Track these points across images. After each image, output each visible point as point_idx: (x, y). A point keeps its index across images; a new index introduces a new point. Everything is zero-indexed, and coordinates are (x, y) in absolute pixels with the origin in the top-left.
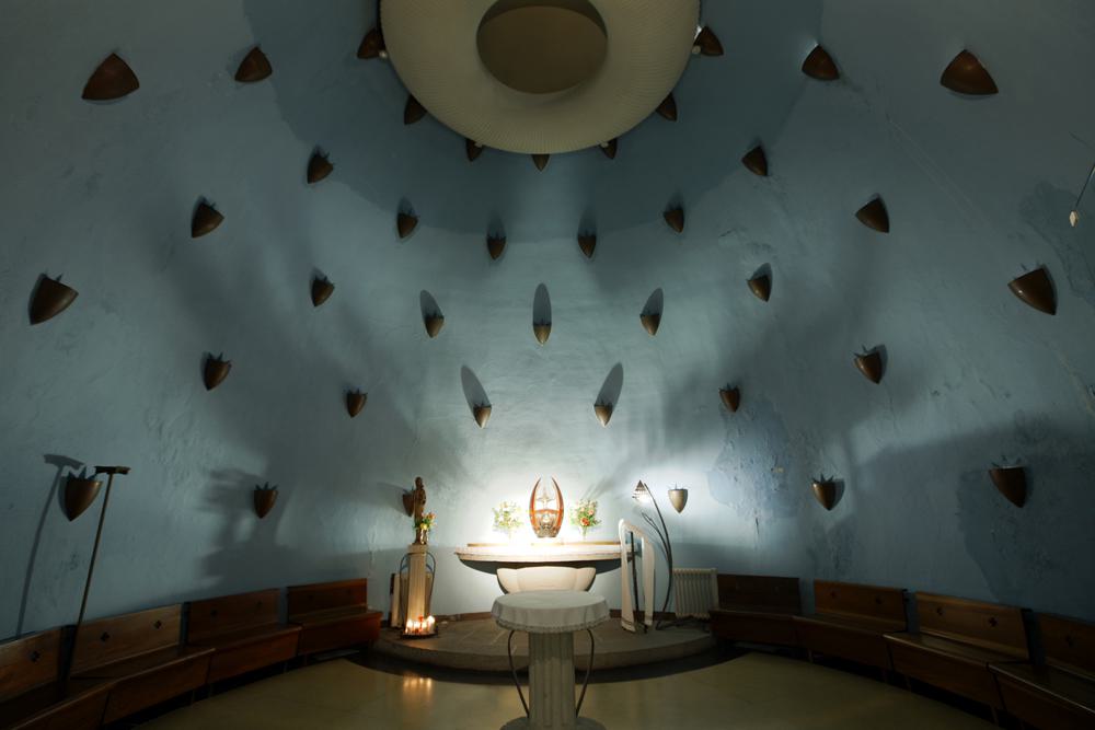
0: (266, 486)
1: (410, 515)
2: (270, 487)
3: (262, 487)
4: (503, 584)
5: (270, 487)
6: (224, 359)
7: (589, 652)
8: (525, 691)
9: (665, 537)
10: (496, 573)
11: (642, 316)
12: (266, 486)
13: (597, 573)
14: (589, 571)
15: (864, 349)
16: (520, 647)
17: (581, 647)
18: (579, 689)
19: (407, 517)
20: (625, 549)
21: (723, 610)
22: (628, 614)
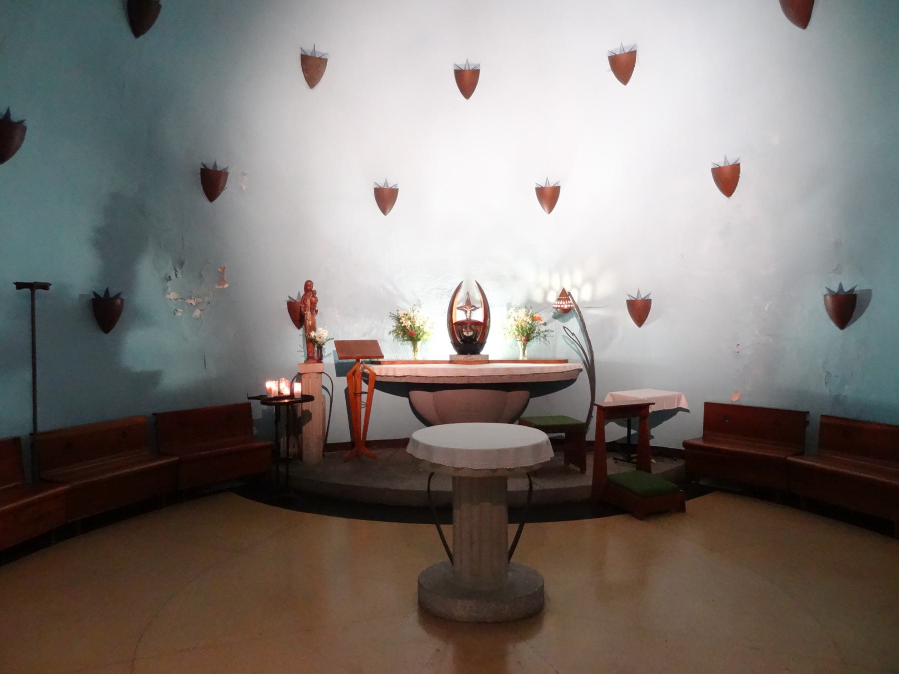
0: (107, 292)
1: (299, 328)
2: (112, 294)
3: (102, 295)
4: (417, 408)
5: (112, 294)
6: (15, 117)
7: (527, 488)
8: (446, 529)
9: (577, 350)
10: (408, 396)
11: (314, 397)
12: (107, 292)
13: (532, 396)
14: (523, 394)
15: (394, 326)
16: (443, 485)
17: (517, 485)
18: (513, 528)
19: (296, 329)
20: (577, 363)
21: (705, 445)
22: (380, 360)
